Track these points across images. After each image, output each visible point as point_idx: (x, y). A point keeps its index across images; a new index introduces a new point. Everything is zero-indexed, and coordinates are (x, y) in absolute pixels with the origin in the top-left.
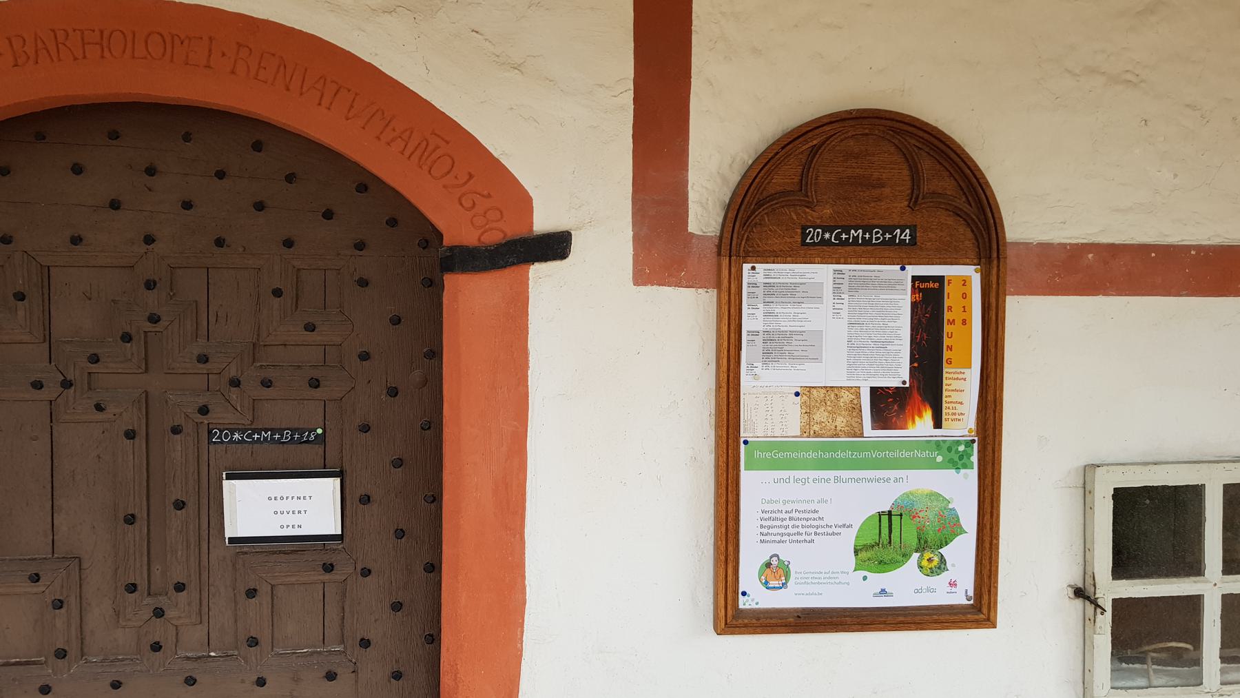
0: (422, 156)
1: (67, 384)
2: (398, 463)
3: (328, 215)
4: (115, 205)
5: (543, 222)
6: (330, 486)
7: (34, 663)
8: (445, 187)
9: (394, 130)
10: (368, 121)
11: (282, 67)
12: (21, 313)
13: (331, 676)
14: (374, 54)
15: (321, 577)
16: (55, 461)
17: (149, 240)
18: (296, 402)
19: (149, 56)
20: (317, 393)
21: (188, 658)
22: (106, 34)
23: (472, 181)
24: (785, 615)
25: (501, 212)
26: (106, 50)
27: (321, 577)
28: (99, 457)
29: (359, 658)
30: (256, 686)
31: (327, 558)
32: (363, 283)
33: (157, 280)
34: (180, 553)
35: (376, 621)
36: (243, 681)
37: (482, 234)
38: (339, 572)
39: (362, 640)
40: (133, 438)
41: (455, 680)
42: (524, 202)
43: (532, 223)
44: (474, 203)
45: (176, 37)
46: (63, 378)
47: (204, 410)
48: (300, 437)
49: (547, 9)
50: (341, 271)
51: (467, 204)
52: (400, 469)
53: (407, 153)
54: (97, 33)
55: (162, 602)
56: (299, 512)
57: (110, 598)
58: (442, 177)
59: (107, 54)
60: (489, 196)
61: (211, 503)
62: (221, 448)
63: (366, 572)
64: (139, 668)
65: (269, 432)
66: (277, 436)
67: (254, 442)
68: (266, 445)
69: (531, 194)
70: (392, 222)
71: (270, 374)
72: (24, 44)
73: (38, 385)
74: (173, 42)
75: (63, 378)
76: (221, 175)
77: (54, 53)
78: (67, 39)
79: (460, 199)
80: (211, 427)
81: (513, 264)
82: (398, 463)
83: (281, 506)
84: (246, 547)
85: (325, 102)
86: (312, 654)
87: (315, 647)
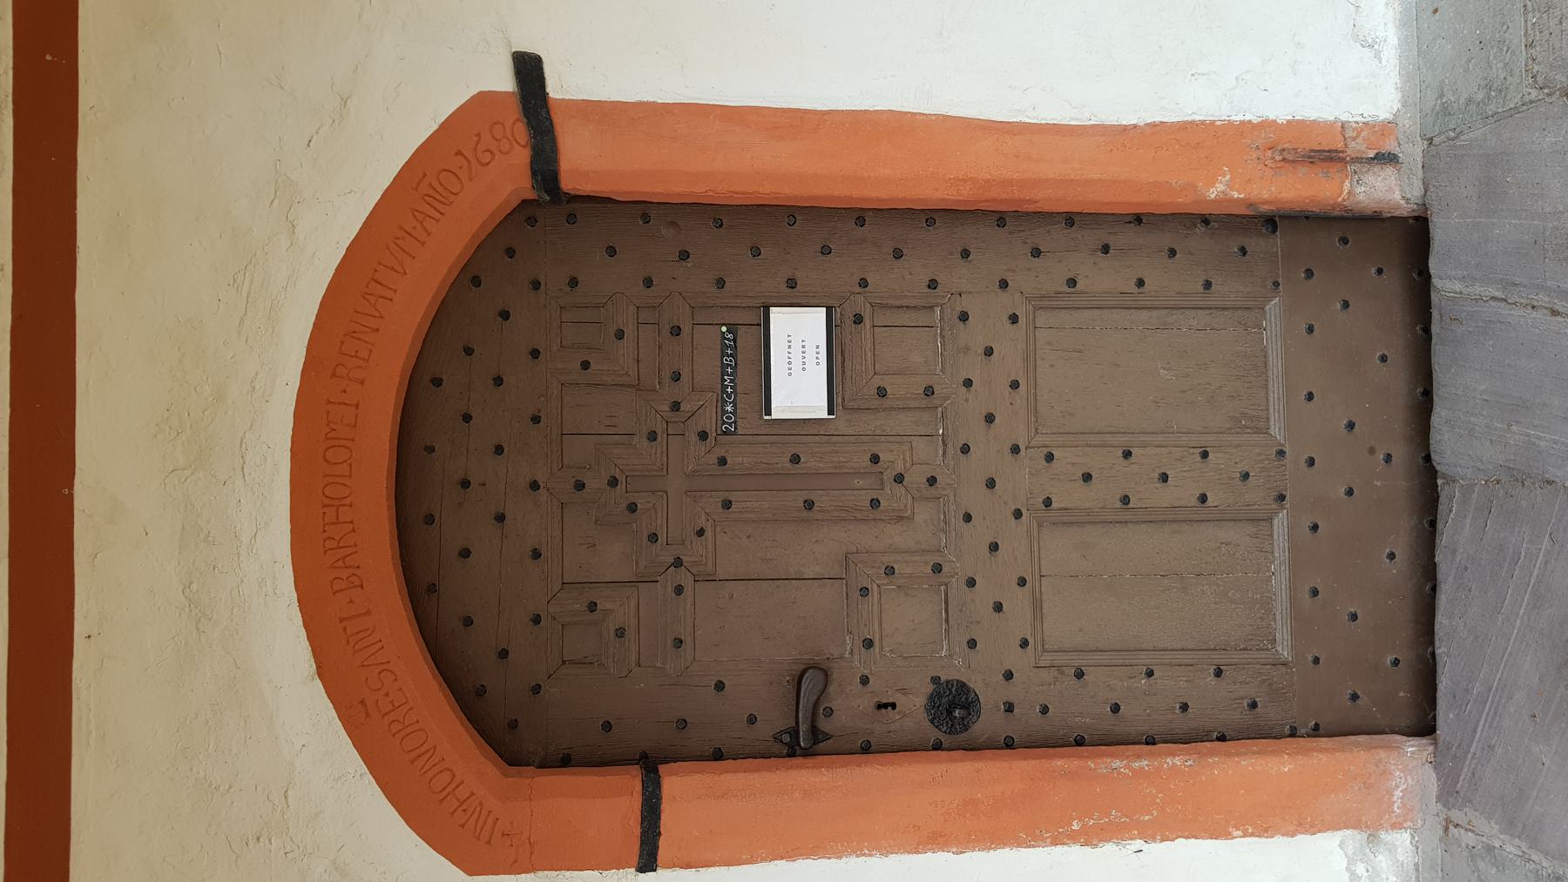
0: (440, 202)
1: (678, 563)
2: (756, 252)
3: (505, 315)
4: (500, 518)
5: (504, 81)
6: (776, 314)
7: (946, 595)
8: (471, 180)
9: (414, 228)
10: (408, 253)
11: (354, 335)
12: (609, 606)
13: (964, 317)
14: (338, 245)
15: (868, 327)
16: (753, 577)
17: (534, 486)
18: (695, 352)
19: (348, 462)
20: (686, 329)
21: (944, 453)
22: (327, 501)
23: (464, 152)
24: (1411, 743)
25: (495, 123)
26: (343, 503)
27: (868, 327)
28: (749, 537)
29: (946, 290)
30: (971, 389)
31: (849, 321)
32: (573, 282)
33: (574, 479)
34: (841, 459)
35: (911, 274)
36: (967, 400)
37: (519, 144)
38: (863, 309)
39: (929, 287)
40: (730, 502)
41: (964, 181)
42: (483, 101)
43: (505, 92)
44: (488, 150)
45: (328, 436)
46: (672, 567)
47: (703, 436)
48: (730, 348)
49: (283, 69)
50: (562, 305)
51: (486, 157)
52: (762, 249)
53: (437, 215)
54: (326, 510)
55: (889, 476)
56: (803, 347)
57: (885, 527)
58: (461, 183)
59: (347, 501)
60: (478, 135)
61: (794, 432)
62: (740, 422)
63: (863, 283)
64: (952, 498)
65: (726, 377)
66: (729, 370)
67: (734, 392)
68: (738, 381)
69: (475, 93)
70: (510, 252)
71: (666, 374)
72: (340, 578)
73: (679, 590)
74: (334, 439)
75: (672, 567)
76: (467, 418)
77: (350, 551)
78: (334, 539)
79: (483, 165)
80: (719, 432)
81: (548, 112)
82: (756, 252)
83: (797, 365)
84: (838, 400)
85: (389, 294)
86: (942, 336)
87: (936, 335)
